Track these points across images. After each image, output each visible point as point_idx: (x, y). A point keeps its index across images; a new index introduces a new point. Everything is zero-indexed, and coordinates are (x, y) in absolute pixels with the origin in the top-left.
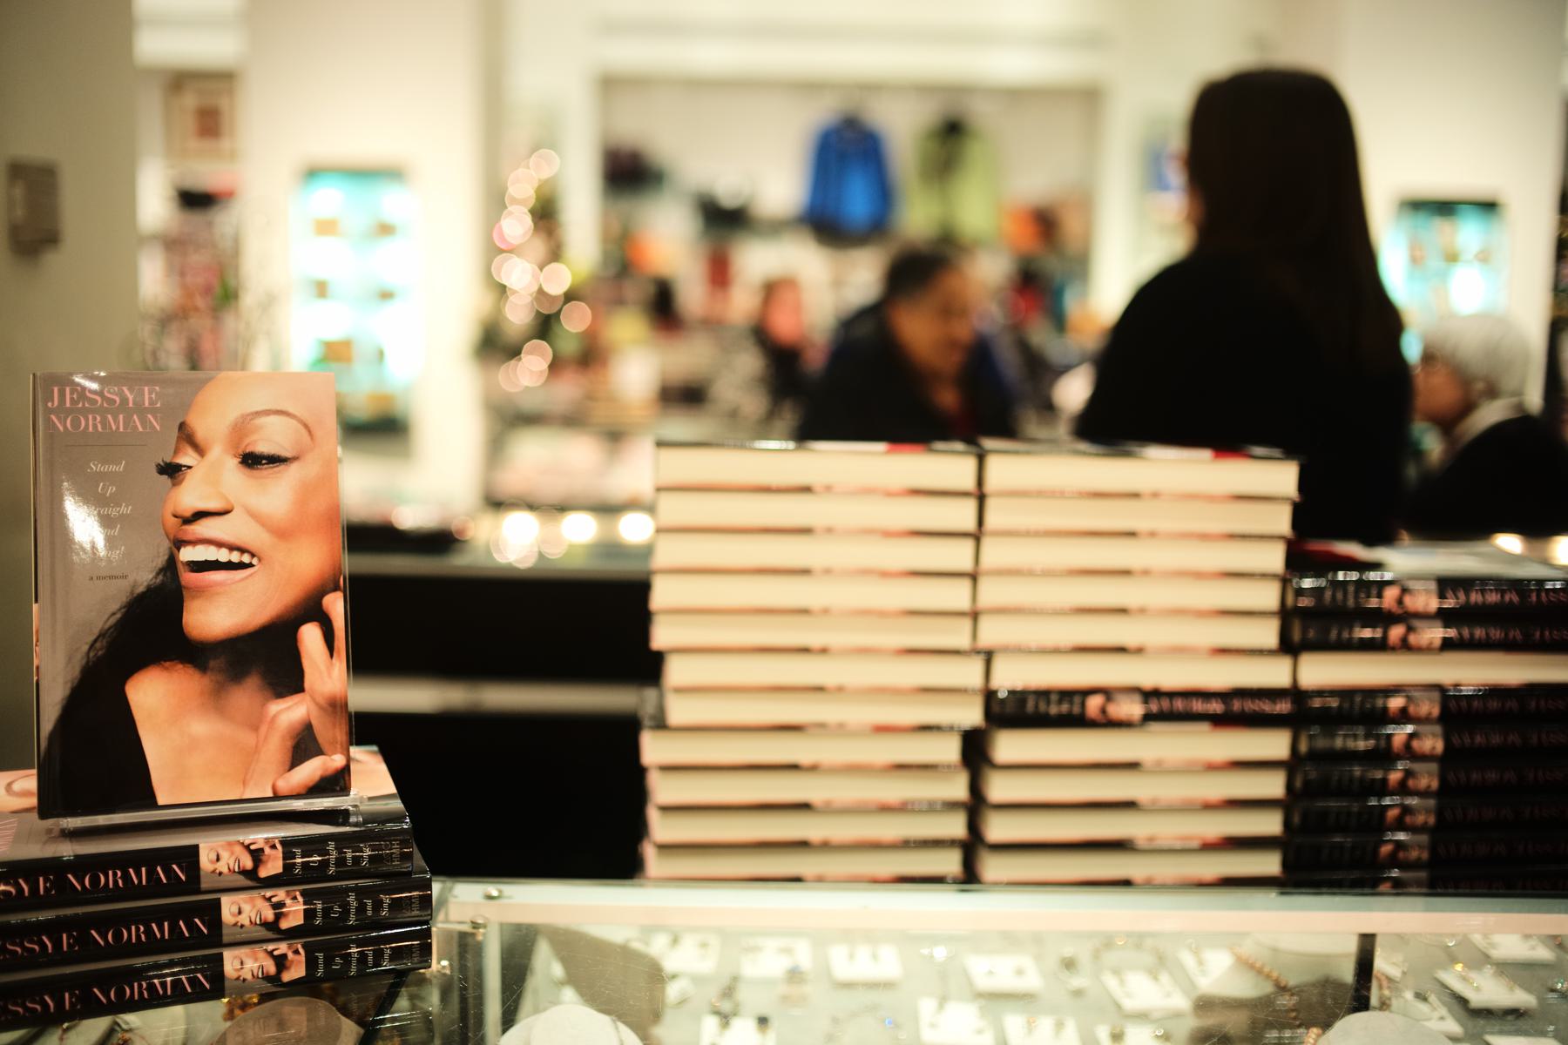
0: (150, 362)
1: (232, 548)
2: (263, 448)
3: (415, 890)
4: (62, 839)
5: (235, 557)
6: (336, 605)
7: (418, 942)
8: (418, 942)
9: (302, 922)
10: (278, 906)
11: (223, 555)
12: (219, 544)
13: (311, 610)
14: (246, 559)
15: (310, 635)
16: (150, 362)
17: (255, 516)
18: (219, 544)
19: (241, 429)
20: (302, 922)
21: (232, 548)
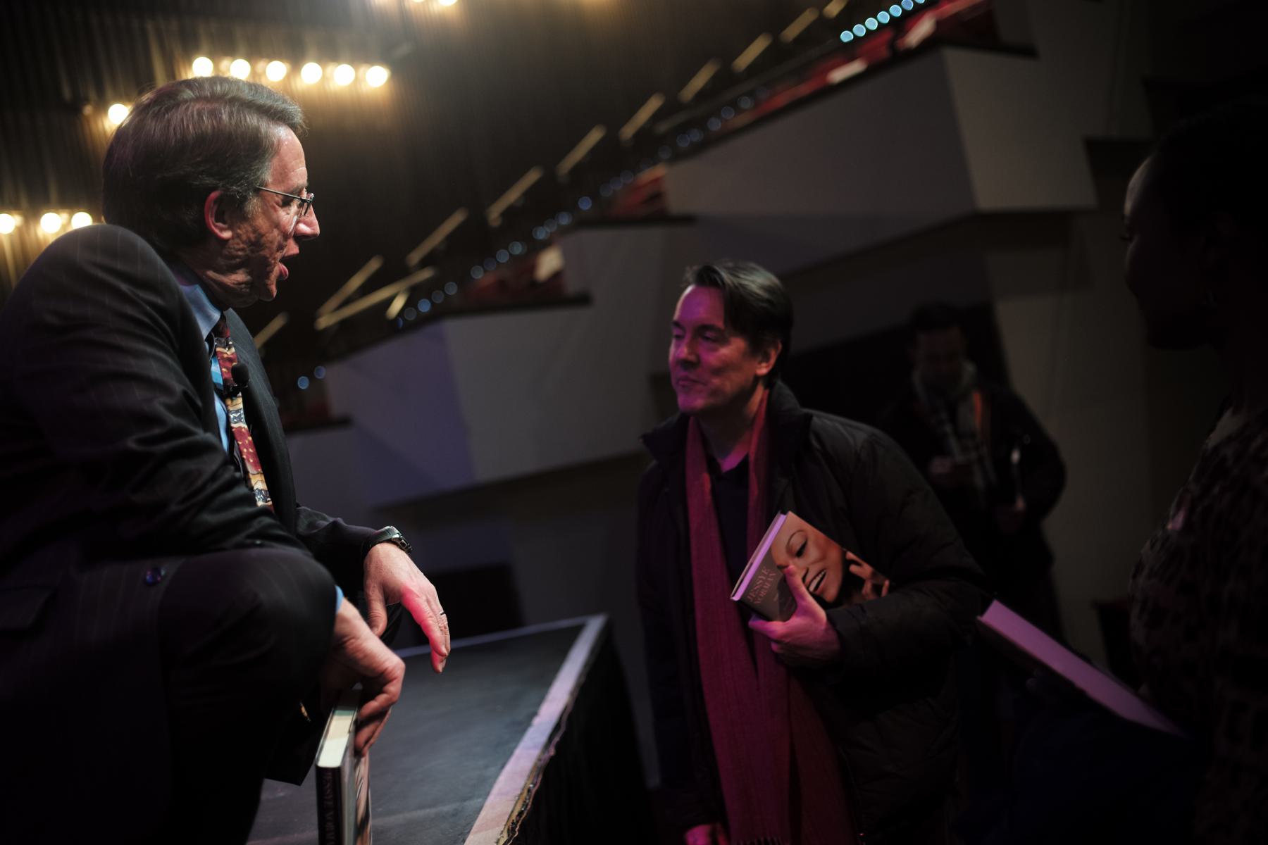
0: (249, 286)
1: (817, 575)
2: (798, 548)
3: (692, 73)
4: (430, 642)
5: (821, 576)
6: (850, 555)
7: (306, 714)
8: (306, 714)
9: (268, 783)
10: (259, 499)
11: (818, 579)
12: (814, 578)
13: (847, 563)
14: (823, 573)
15: (854, 568)
16: (249, 286)
17: (814, 563)
18: (814, 578)
19: (789, 550)
20: (268, 783)
21: (817, 575)
